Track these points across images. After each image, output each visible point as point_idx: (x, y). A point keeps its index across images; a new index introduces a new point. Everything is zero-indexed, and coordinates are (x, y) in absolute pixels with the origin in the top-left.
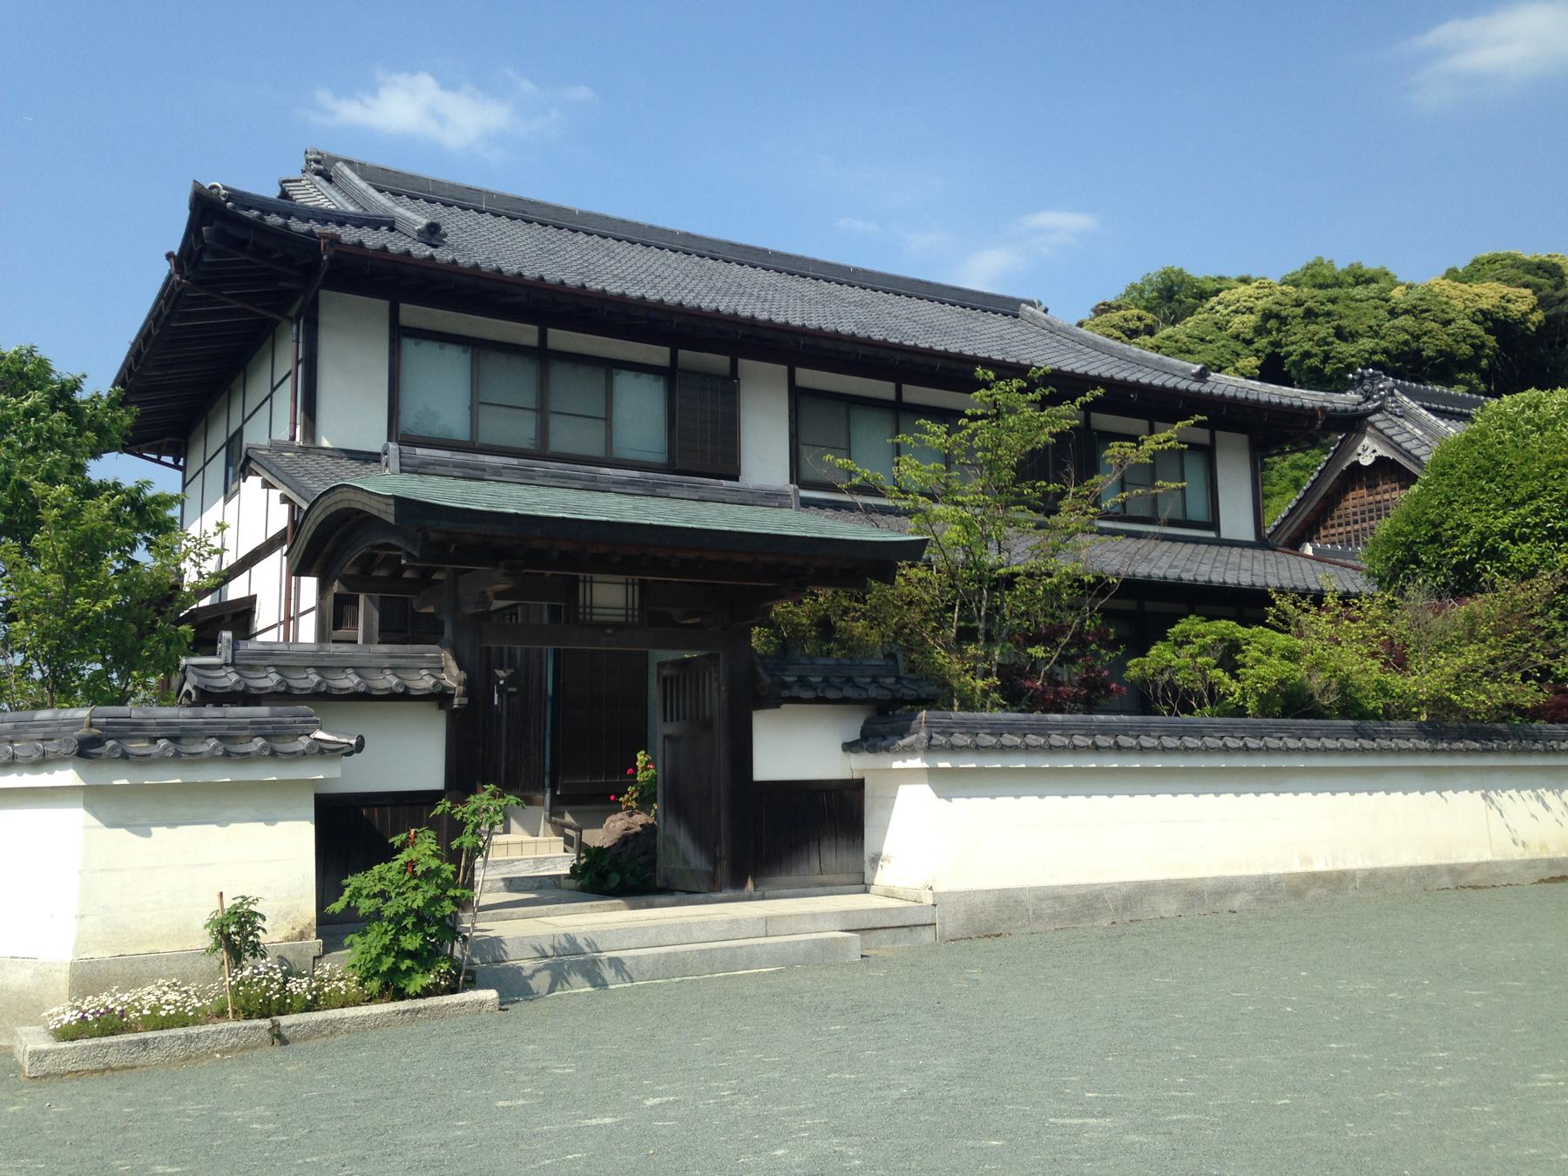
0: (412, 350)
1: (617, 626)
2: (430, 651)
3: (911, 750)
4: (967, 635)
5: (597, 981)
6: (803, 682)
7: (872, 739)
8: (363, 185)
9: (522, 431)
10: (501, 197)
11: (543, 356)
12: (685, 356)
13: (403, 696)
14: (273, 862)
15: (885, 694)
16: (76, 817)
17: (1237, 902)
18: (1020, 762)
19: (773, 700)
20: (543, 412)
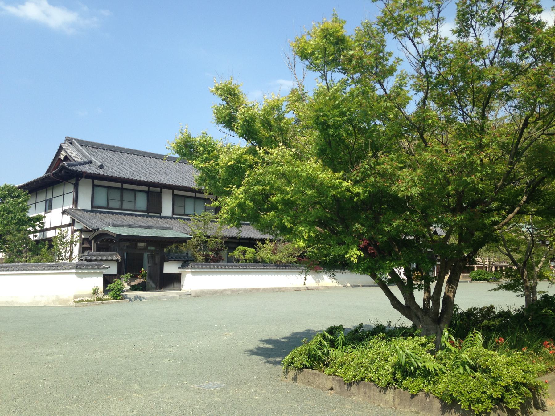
0: (97, 189)
1: (143, 249)
2: (115, 253)
3: (188, 268)
4: (200, 250)
5: (141, 300)
6: (172, 257)
7: (183, 266)
8: (78, 144)
9: (117, 204)
10: (109, 146)
11: (122, 189)
12: (151, 188)
13: (112, 260)
14: (98, 282)
15: (185, 260)
16: (74, 276)
17: (240, 292)
18: (206, 270)
19: (167, 260)
20: (122, 201)
